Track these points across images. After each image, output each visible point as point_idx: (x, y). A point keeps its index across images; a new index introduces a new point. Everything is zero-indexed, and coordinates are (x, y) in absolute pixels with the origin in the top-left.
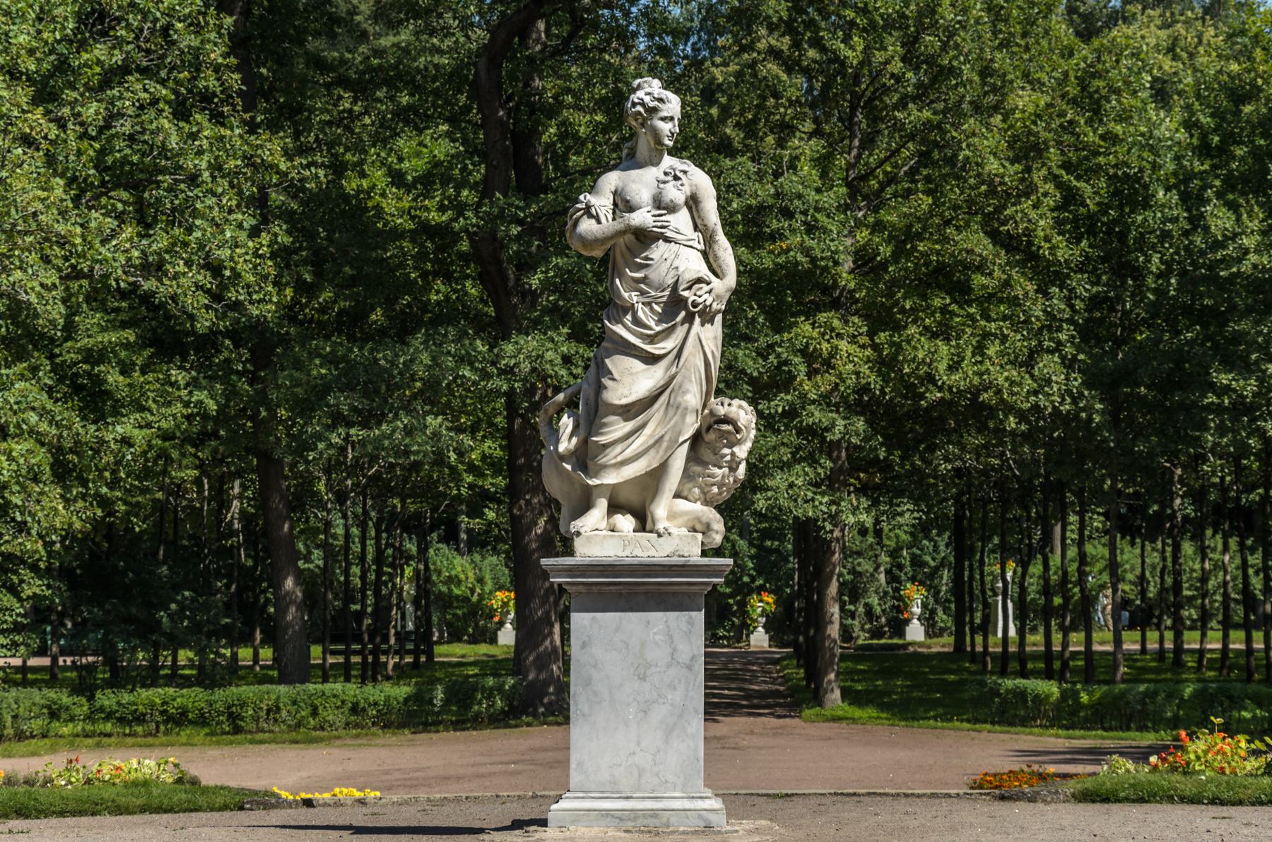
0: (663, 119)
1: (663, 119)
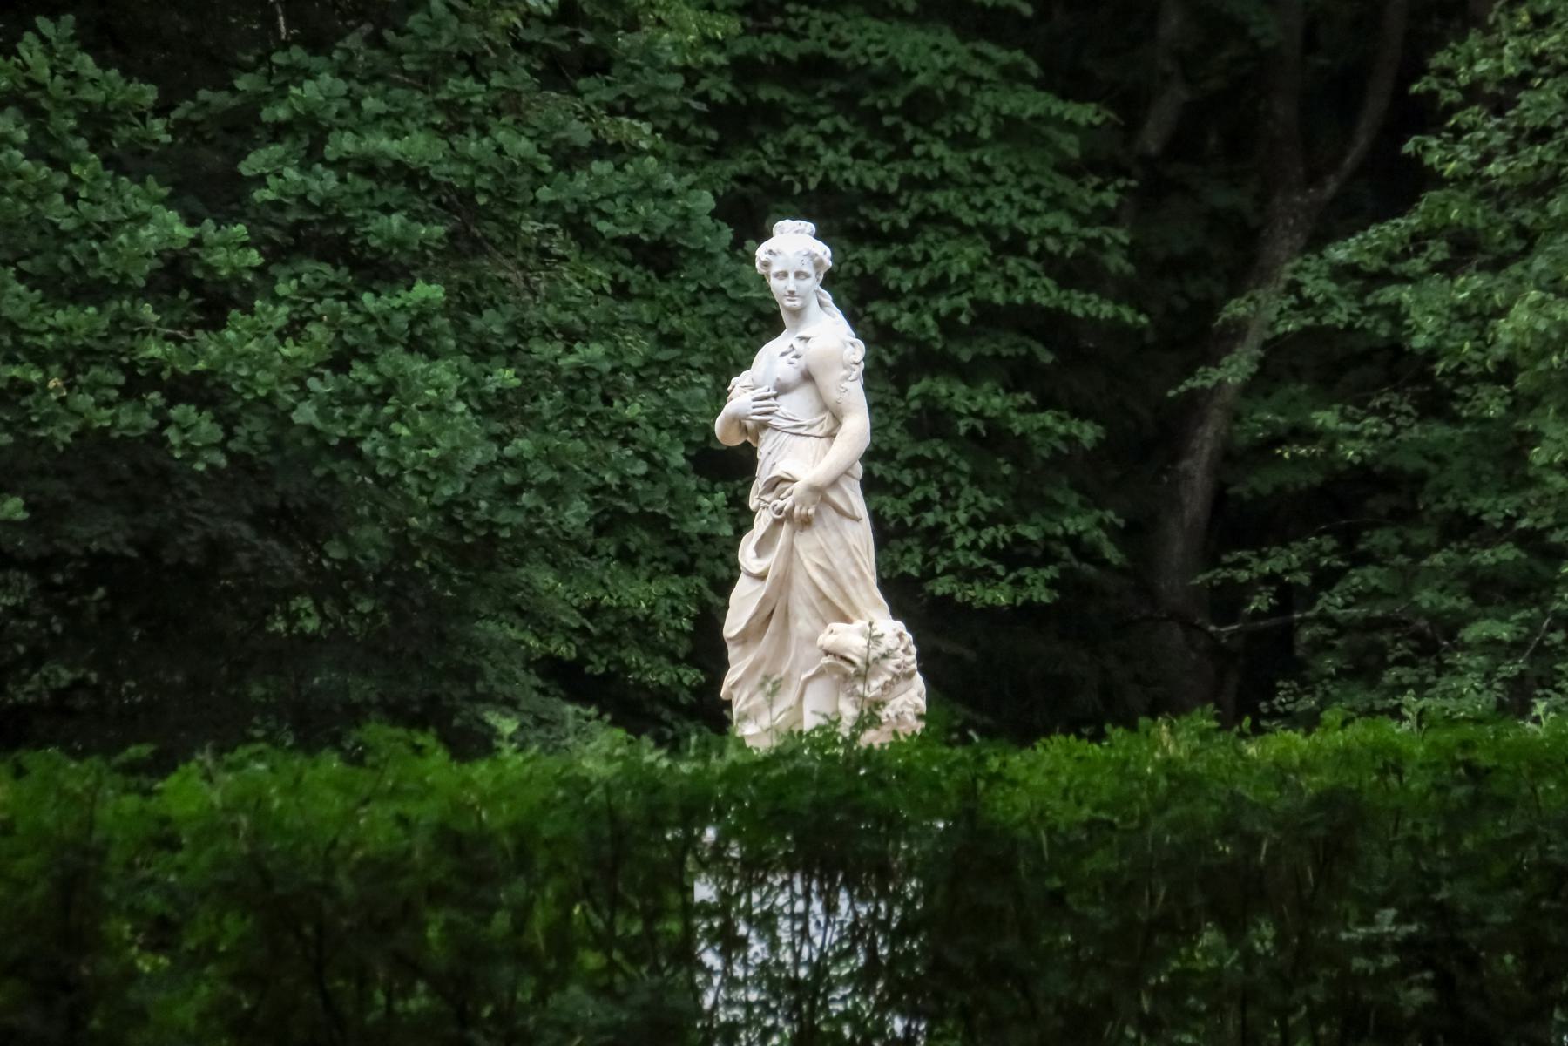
0: (777, 275)
1: (777, 275)
